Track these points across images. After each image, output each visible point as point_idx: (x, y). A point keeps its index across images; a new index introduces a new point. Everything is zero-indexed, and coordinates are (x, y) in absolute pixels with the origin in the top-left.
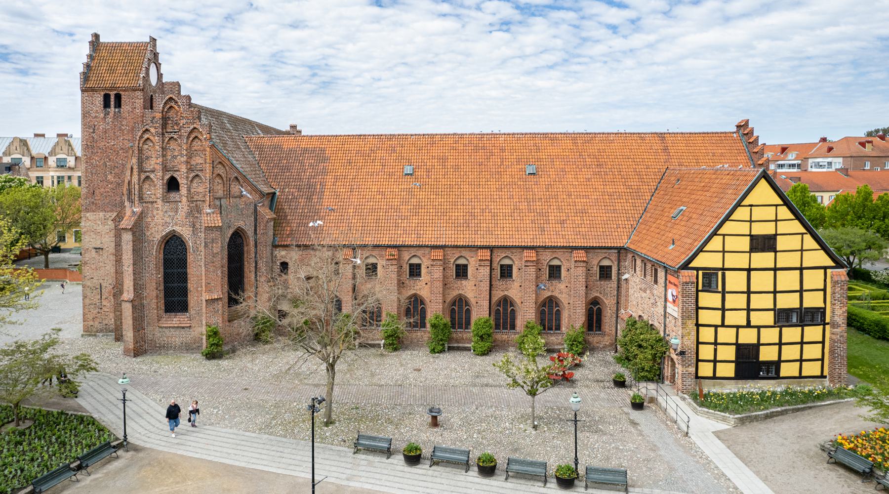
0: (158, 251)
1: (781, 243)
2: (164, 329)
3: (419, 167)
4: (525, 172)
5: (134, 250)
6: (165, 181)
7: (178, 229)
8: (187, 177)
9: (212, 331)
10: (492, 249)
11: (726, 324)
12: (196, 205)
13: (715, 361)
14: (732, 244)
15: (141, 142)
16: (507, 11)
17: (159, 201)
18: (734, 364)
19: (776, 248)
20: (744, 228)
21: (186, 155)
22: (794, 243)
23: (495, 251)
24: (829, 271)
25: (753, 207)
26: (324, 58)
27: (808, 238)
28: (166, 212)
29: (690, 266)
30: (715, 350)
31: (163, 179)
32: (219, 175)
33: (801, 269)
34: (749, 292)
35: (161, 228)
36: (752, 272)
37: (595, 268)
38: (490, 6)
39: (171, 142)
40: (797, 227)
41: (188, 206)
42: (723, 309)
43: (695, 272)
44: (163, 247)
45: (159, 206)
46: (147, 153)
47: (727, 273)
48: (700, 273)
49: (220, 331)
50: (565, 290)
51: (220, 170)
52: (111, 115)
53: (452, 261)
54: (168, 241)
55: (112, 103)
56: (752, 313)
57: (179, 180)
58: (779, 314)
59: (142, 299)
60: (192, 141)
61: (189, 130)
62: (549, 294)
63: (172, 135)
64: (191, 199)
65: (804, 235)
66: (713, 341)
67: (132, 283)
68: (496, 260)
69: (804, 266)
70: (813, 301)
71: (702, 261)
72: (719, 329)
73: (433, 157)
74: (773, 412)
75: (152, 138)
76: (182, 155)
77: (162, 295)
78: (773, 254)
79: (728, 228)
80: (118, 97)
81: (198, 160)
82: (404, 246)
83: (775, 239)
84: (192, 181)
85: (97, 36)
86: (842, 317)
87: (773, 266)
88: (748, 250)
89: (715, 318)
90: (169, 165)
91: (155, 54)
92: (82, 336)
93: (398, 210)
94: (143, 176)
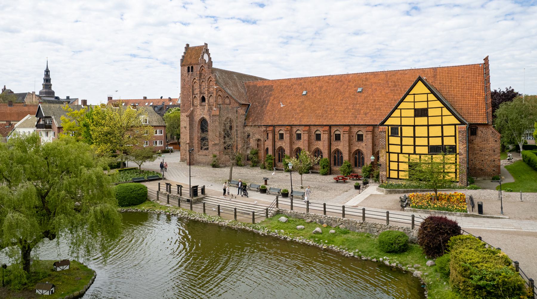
1: (431, 112)
3: (309, 92)
7: (204, 116)
8: (208, 96)
10: (330, 126)
11: (403, 152)
13: (398, 171)
14: (405, 113)
15: (193, 83)
16: (510, 7)
17: (199, 106)
19: (428, 115)
20: (411, 105)
22: (438, 112)
24: (457, 126)
25: (415, 95)
26: (379, 50)
27: (445, 109)
29: (385, 124)
30: (398, 165)
31: (200, 97)
32: (219, 95)
33: (442, 126)
34: (414, 137)
36: (416, 127)
38: (493, 4)
39: (203, 83)
40: (439, 104)
42: (401, 145)
43: (387, 127)
44: (200, 123)
47: (403, 127)
48: (390, 127)
51: (220, 93)
52: (190, 75)
53: (314, 132)
55: (190, 70)
56: (416, 147)
58: (431, 148)
59: (193, 143)
61: (208, 77)
62: (357, 148)
63: (203, 80)
64: (209, 105)
65: (443, 108)
68: (333, 131)
69: (443, 124)
70: (449, 142)
71: (390, 122)
73: (317, 87)
74: (408, 190)
78: (427, 118)
79: (402, 106)
80: (192, 67)
82: (294, 125)
84: (209, 98)
85: (188, 45)
86: (463, 150)
87: (427, 124)
88: (413, 116)
89: (397, 149)
90: (202, 92)
92: (180, 161)
93: (295, 110)
94: (194, 97)
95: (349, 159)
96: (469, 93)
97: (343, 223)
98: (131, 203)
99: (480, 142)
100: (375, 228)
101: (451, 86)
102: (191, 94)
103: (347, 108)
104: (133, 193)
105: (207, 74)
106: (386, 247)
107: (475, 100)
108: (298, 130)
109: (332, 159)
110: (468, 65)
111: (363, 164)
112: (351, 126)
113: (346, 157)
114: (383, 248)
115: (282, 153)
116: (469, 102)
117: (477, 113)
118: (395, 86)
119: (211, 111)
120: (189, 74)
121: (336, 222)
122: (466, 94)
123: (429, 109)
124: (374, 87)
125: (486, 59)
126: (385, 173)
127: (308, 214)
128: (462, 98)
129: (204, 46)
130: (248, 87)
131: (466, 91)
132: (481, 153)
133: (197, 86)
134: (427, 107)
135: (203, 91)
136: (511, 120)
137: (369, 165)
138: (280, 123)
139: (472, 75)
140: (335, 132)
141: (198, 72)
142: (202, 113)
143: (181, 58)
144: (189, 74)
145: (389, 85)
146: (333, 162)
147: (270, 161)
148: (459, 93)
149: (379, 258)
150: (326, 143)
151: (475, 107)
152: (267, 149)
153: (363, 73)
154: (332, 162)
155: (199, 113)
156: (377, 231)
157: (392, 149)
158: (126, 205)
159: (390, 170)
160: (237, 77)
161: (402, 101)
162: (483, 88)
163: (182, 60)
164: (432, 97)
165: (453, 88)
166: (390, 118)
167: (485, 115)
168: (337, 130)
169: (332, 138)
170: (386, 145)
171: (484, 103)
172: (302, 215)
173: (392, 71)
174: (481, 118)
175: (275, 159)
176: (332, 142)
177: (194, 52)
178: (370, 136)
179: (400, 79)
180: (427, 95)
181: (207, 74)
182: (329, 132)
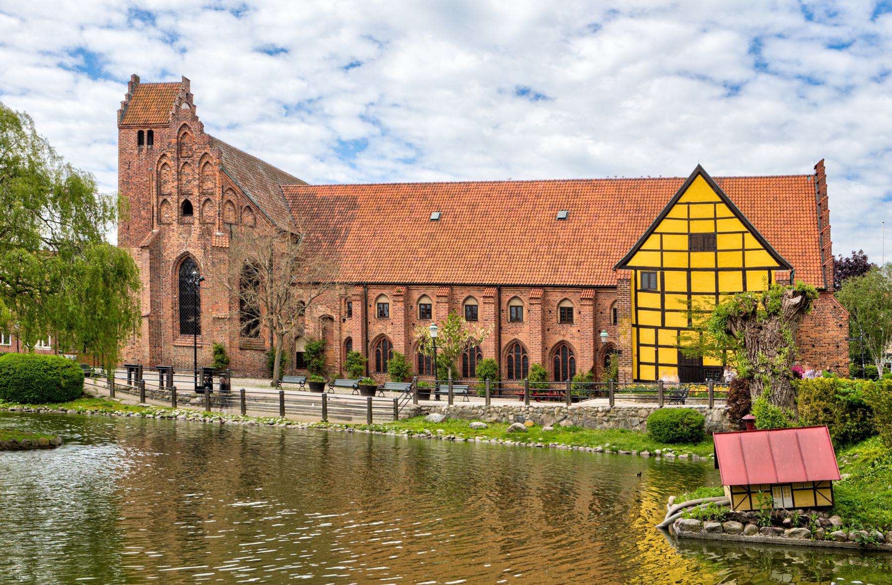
0: (173, 271)
1: (722, 242)
2: (179, 349)
3: (446, 214)
4: (556, 217)
5: (151, 267)
6: (180, 205)
7: (191, 250)
8: (199, 201)
9: (217, 348)
10: (500, 287)
12: (207, 228)
13: (657, 365)
17: (175, 223)
18: (676, 369)
19: (716, 248)
20: (682, 227)
21: (199, 179)
22: (735, 242)
23: (504, 290)
24: (773, 272)
27: (749, 237)
28: (181, 234)
29: (629, 264)
30: (657, 352)
31: (178, 202)
32: (229, 201)
33: (744, 270)
35: (176, 249)
37: (608, 310)
39: (186, 167)
40: (737, 225)
41: (200, 228)
42: (663, 310)
43: (633, 271)
44: (178, 268)
45: (175, 228)
46: (165, 178)
47: (666, 273)
48: (639, 272)
49: (227, 351)
50: (577, 335)
52: (144, 151)
53: (461, 301)
54: (183, 264)
57: (193, 204)
60: (204, 166)
61: (201, 155)
62: (561, 338)
63: (186, 160)
64: (203, 223)
66: (653, 343)
67: (149, 299)
71: (639, 260)
72: (660, 331)
73: (464, 204)
75: (168, 162)
76: (194, 179)
77: (178, 315)
79: (664, 226)
80: (151, 134)
81: (209, 185)
83: (715, 238)
84: (204, 205)
87: (714, 266)
89: (654, 318)
90: (184, 189)
91: (187, 94)
94: (161, 200)
95: (544, 362)
96: (789, 230)
97: (569, 417)
98: (47, 395)
99: (812, 328)
100: (635, 416)
101: (753, 215)
102: (155, 193)
103: (535, 251)
104: (50, 372)
105: (196, 147)
106: (666, 432)
107: (800, 244)
108: (424, 296)
109: (504, 364)
110: (786, 177)
111: (573, 374)
112: (548, 289)
113: (535, 358)
114: (660, 435)
115: (385, 351)
116: (790, 247)
117: (805, 268)
118: (638, 210)
119: (209, 238)
120: (140, 150)
121: (553, 415)
122: (783, 233)
123: (713, 253)
124: (593, 210)
125: (820, 167)
126: (631, 369)
127: (489, 408)
128: (776, 240)
129: (181, 83)
130: (294, 197)
131: (782, 226)
132: (814, 349)
133: (169, 175)
134: (714, 231)
135: (188, 188)
136: (863, 311)
137: (588, 375)
138: (380, 279)
139: (794, 196)
140: (510, 301)
141: (174, 141)
142: (183, 241)
143: (119, 107)
144: (140, 150)
145: (626, 209)
146: (507, 371)
147: (355, 366)
148: (769, 229)
149: (653, 450)
150: (492, 327)
151: (801, 258)
152: (349, 341)
153: (568, 181)
154: (504, 371)
155: (176, 243)
156: (641, 423)
157: (645, 318)
158: (34, 399)
159: (639, 363)
160: (264, 170)
161: (664, 216)
162: (816, 222)
163: (121, 111)
164: (723, 210)
165: (756, 219)
166: (639, 253)
167: (819, 272)
168: (515, 297)
169: (503, 314)
170: (630, 308)
171: (818, 250)
172: (475, 411)
173: (630, 180)
174: (813, 279)
175: (367, 363)
176: (503, 325)
177: (152, 96)
178: (588, 310)
179: (648, 196)
180: (715, 206)
181: (196, 147)
182: (497, 300)
